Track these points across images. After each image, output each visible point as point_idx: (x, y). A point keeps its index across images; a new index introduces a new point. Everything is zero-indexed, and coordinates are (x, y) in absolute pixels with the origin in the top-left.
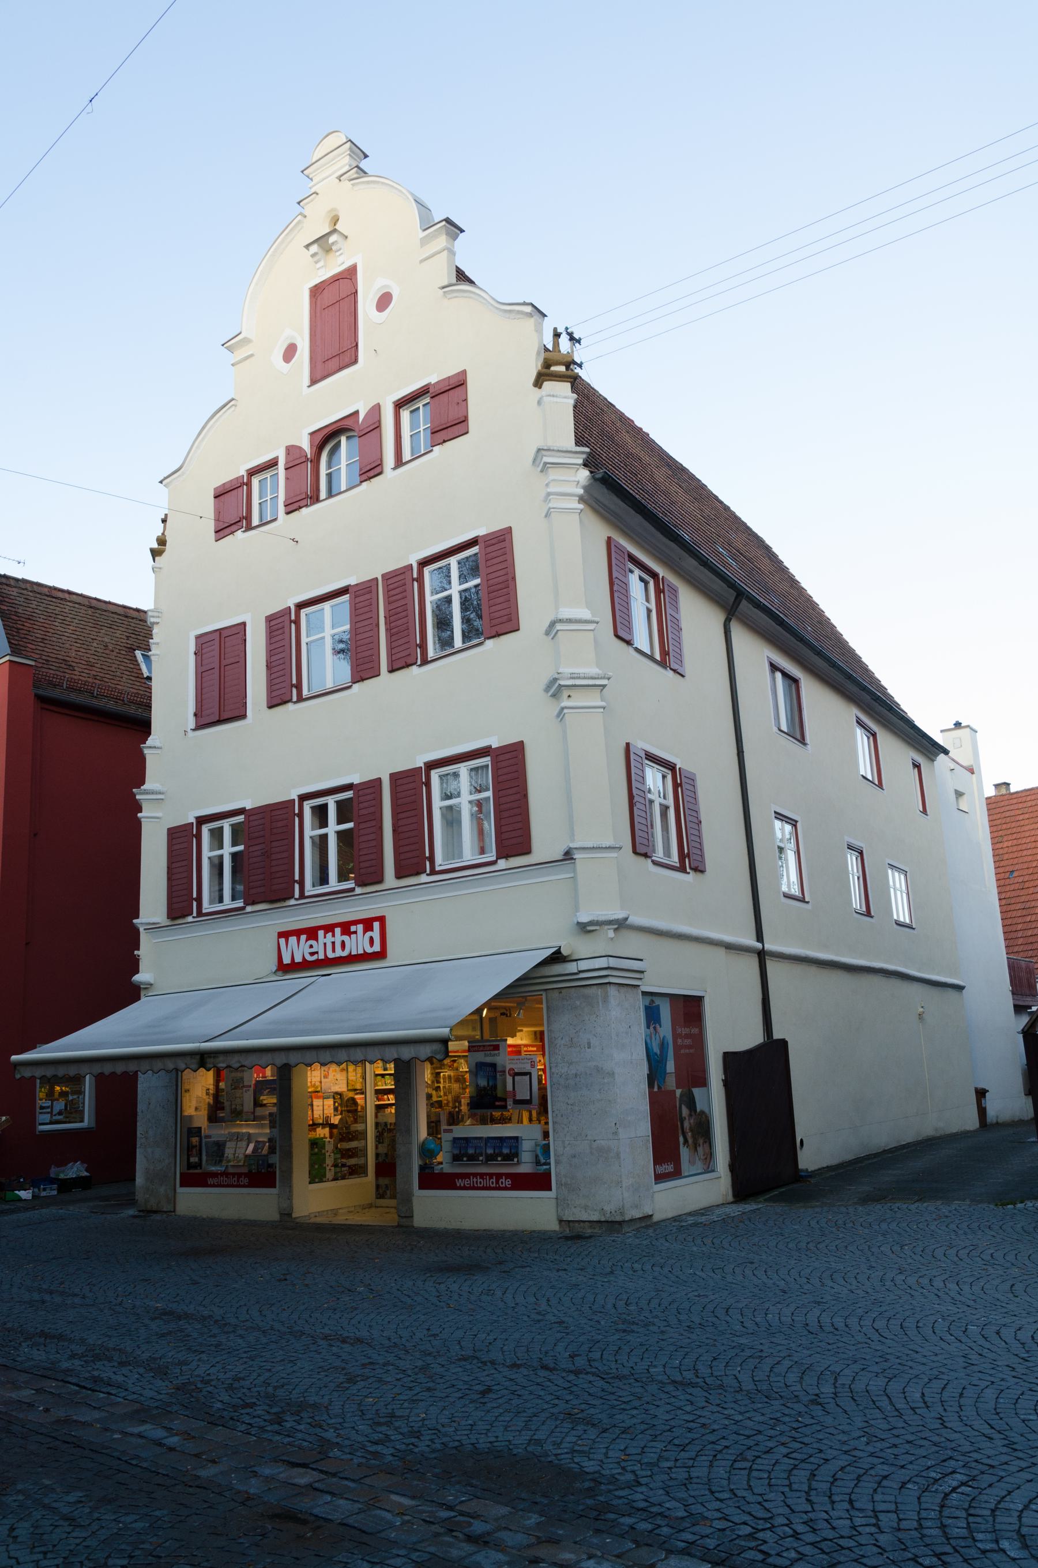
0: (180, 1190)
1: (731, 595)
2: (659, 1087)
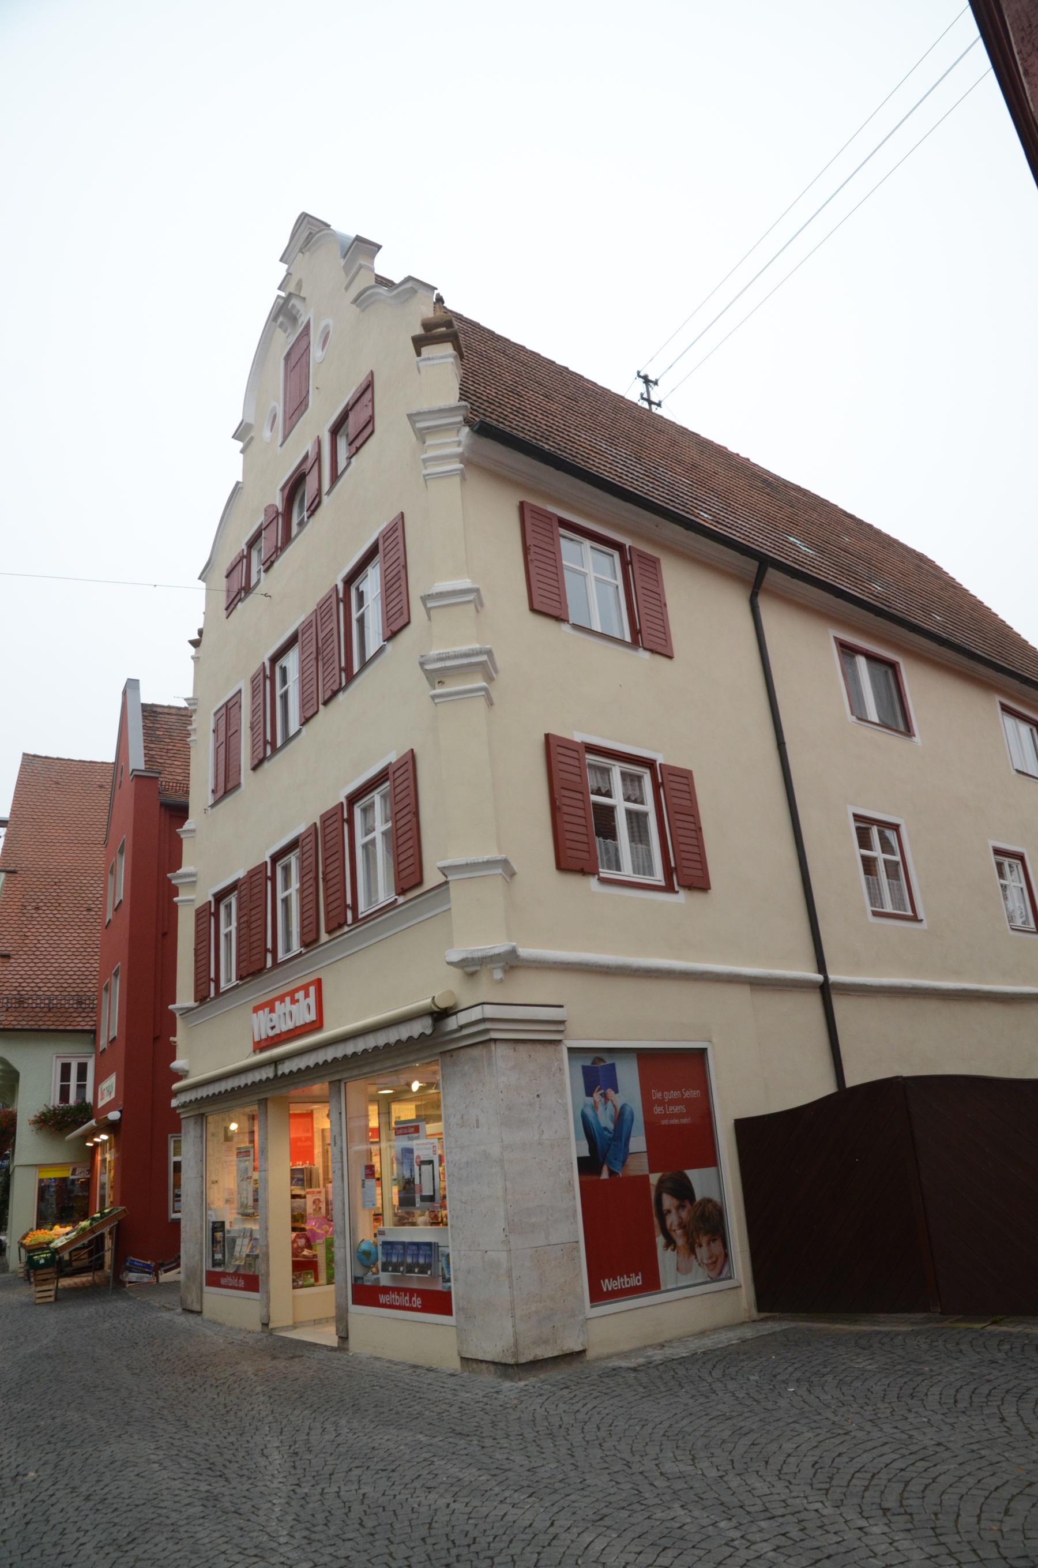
0: (207, 1289)
1: (753, 565)
2: (612, 1173)
